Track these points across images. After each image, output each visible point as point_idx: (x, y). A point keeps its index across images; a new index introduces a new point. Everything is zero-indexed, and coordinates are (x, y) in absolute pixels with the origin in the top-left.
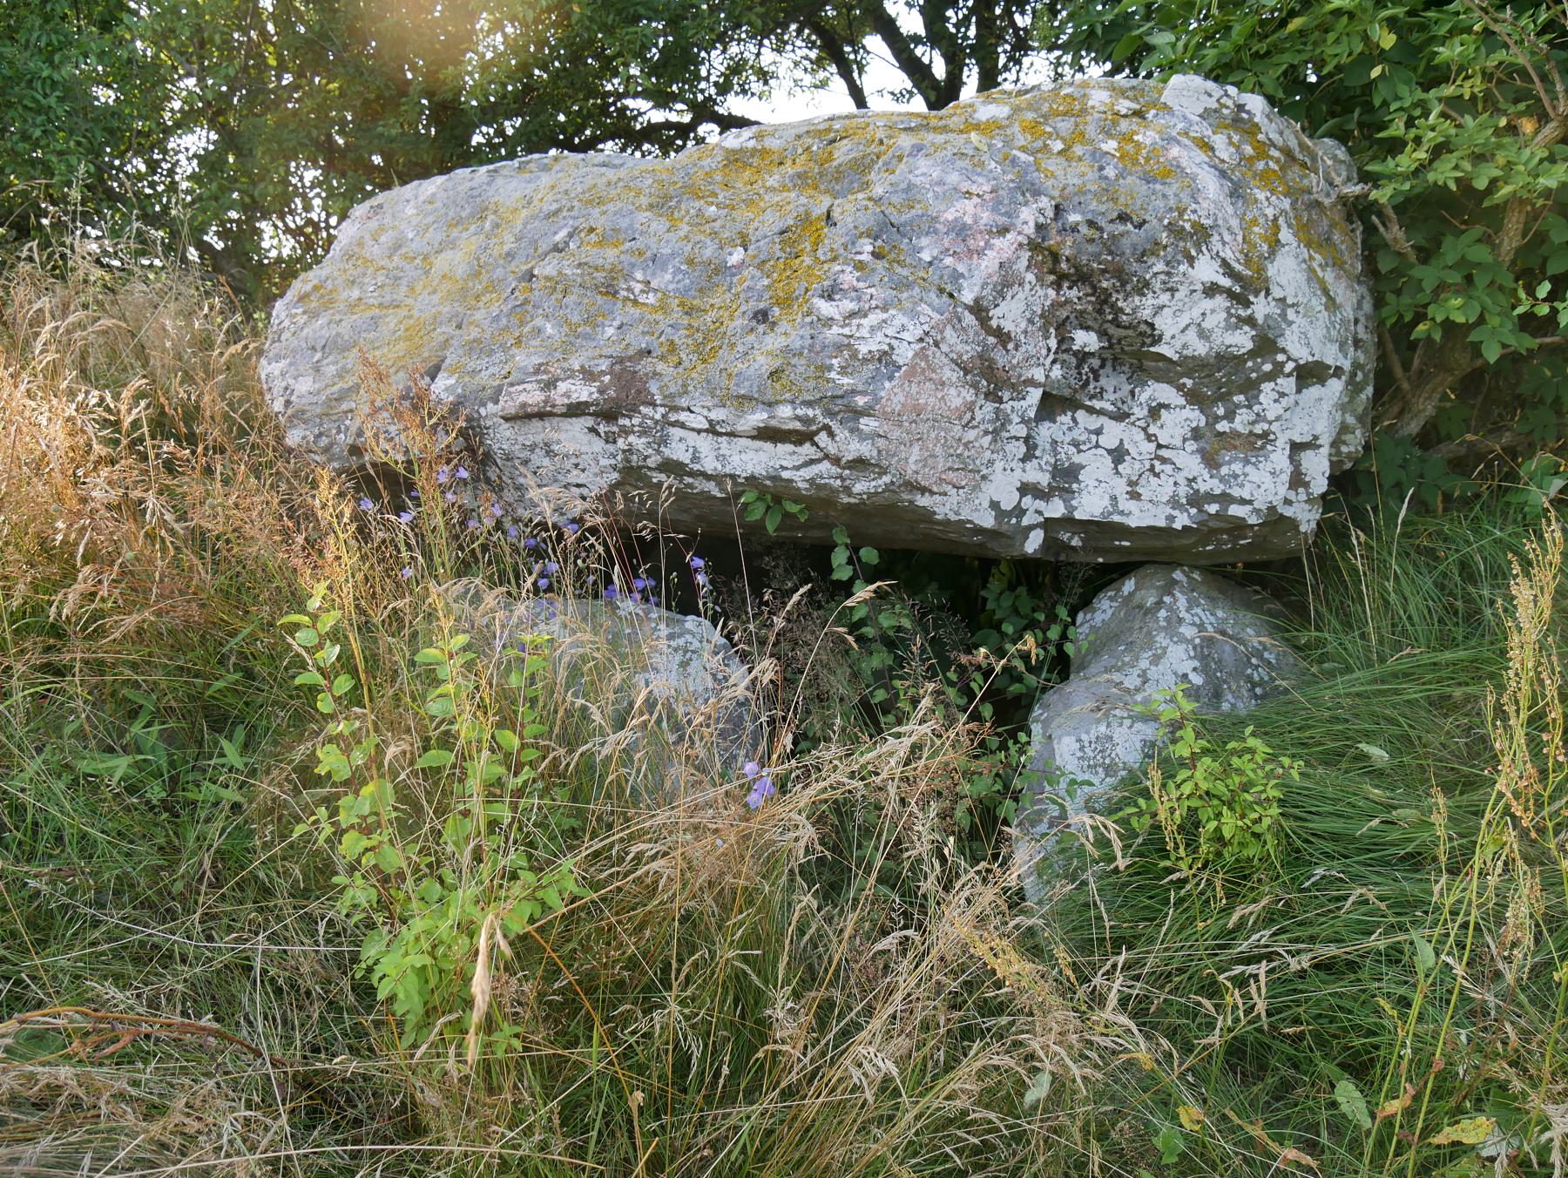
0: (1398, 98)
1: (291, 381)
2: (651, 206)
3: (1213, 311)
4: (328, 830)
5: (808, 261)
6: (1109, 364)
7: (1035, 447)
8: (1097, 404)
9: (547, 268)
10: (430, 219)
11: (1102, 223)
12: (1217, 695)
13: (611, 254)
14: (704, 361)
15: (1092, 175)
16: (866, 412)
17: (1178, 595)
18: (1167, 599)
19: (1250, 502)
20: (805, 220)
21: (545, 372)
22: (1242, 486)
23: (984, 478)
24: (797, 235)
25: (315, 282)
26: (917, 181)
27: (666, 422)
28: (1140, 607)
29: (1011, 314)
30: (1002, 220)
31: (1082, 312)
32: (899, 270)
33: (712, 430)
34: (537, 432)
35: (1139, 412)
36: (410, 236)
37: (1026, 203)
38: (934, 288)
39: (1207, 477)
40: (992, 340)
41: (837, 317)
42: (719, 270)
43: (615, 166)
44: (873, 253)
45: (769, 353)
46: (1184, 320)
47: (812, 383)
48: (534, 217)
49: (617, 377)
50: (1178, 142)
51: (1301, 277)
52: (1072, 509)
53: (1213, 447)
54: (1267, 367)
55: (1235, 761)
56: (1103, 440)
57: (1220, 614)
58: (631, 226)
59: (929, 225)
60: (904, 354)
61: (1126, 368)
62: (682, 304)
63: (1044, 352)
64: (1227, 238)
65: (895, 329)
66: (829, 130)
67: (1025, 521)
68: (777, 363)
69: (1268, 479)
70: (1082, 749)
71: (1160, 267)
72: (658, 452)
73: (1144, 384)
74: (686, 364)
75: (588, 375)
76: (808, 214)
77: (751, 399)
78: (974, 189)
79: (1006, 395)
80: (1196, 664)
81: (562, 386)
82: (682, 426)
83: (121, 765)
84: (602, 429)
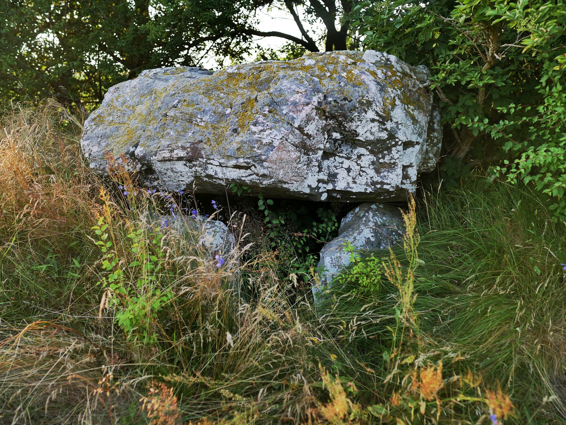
0: (441, 54)
1: (91, 148)
2: (203, 93)
3: (374, 127)
4: (106, 283)
5: (249, 113)
6: (344, 142)
7: (322, 168)
8: (341, 155)
9: (171, 113)
10: (135, 94)
11: (338, 101)
12: (379, 244)
13: (191, 109)
14: (218, 144)
15: (337, 85)
16: (265, 161)
17: (370, 213)
18: (367, 214)
19: (390, 184)
20: (249, 100)
21: (171, 147)
22: (387, 179)
23: (305, 178)
24: (249, 103)
25: (98, 114)
26: (283, 88)
27: (206, 163)
28: (359, 216)
29: (311, 129)
30: (307, 101)
31: (334, 127)
32: (276, 116)
33: (221, 165)
34: (168, 165)
35: (354, 157)
36: (128, 99)
37: (315, 95)
38: (286, 123)
39: (376, 176)
40: (305, 137)
41: (257, 131)
42: (224, 115)
43: (193, 78)
44: (269, 111)
45: (237, 142)
46: (366, 129)
47: (249, 152)
48: (167, 96)
49: (192, 149)
50: (365, 73)
51: (404, 115)
52: (335, 187)
53: (378, 167)
54: (393, 143)
55: (369, 263)
56: (343, 165)
57: (384, 218)
58: (197, 100)
59: (285, 102)
60: (276, 143)
61: (350, 144)
62: (212, 126)
63: (323, 139)
64: (378, 104)
65: (273, 135)
66: (260, 67)
67: (320, 191)
68: (239, 145)
69: (395, 177)
70: (332, 260)
71: (356, 114)
72: (205, 172)
73: (356, 148)
74: (213, 145)
75: (184, 148)
76: (250, 98)
77: (231, 156)
78: (300, 91)
79: (311, 153)
80: (373, 234)
81: (176, 152)
82: (212, 164)
83: (44, 267)
84: (188, 164)
